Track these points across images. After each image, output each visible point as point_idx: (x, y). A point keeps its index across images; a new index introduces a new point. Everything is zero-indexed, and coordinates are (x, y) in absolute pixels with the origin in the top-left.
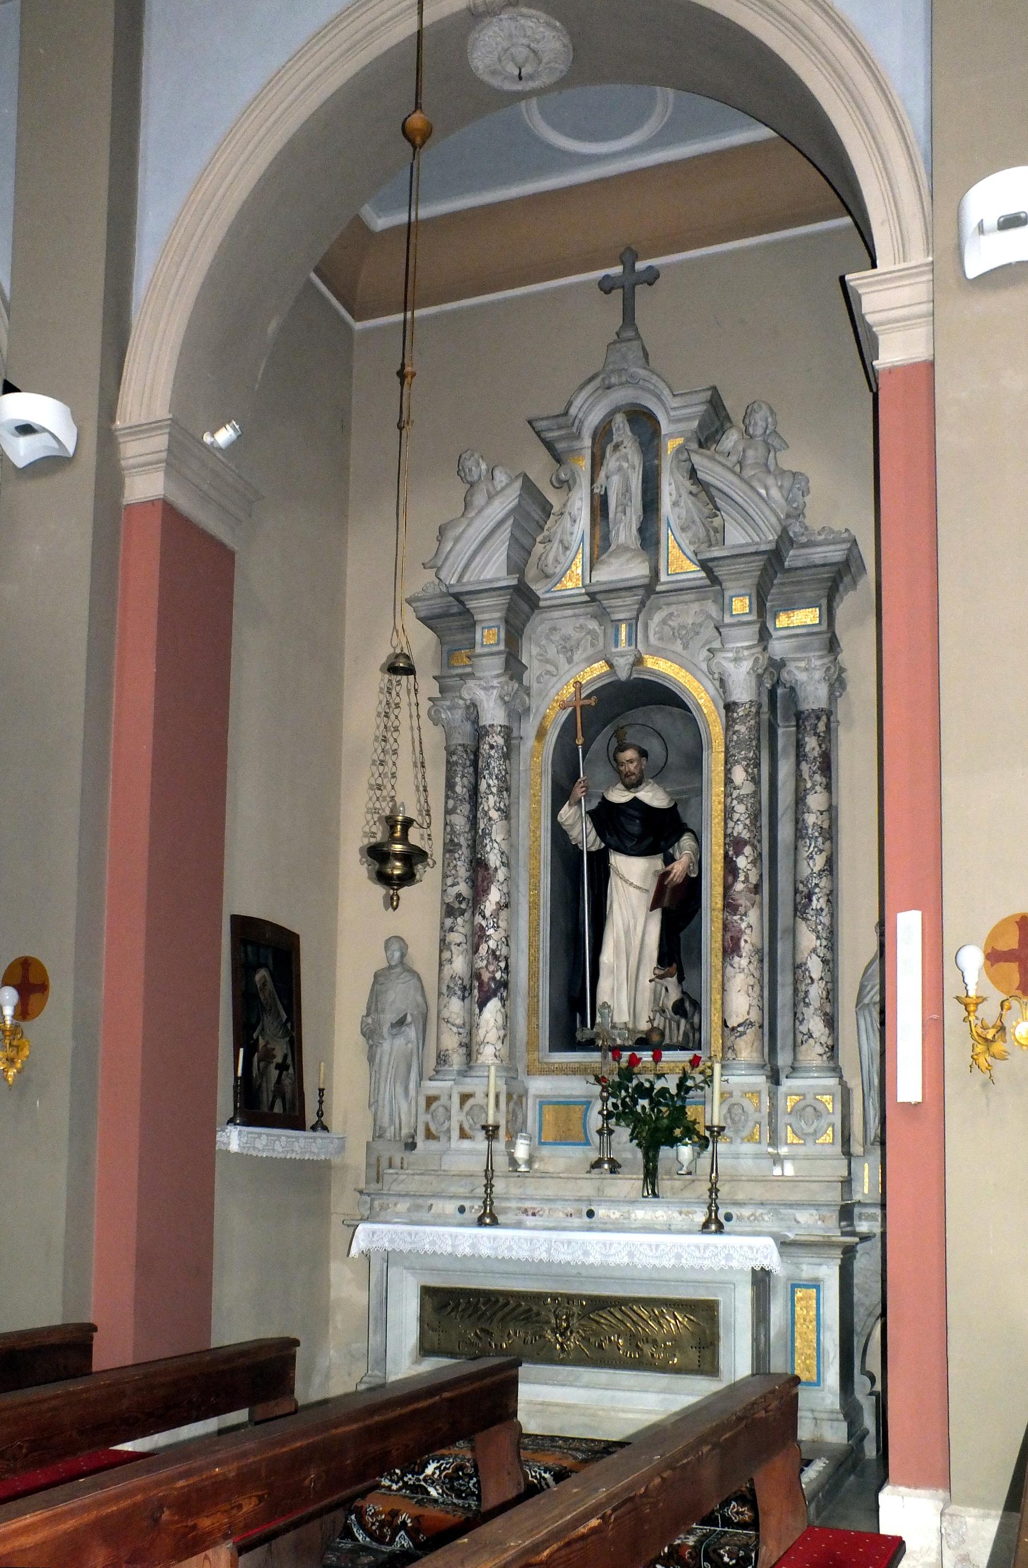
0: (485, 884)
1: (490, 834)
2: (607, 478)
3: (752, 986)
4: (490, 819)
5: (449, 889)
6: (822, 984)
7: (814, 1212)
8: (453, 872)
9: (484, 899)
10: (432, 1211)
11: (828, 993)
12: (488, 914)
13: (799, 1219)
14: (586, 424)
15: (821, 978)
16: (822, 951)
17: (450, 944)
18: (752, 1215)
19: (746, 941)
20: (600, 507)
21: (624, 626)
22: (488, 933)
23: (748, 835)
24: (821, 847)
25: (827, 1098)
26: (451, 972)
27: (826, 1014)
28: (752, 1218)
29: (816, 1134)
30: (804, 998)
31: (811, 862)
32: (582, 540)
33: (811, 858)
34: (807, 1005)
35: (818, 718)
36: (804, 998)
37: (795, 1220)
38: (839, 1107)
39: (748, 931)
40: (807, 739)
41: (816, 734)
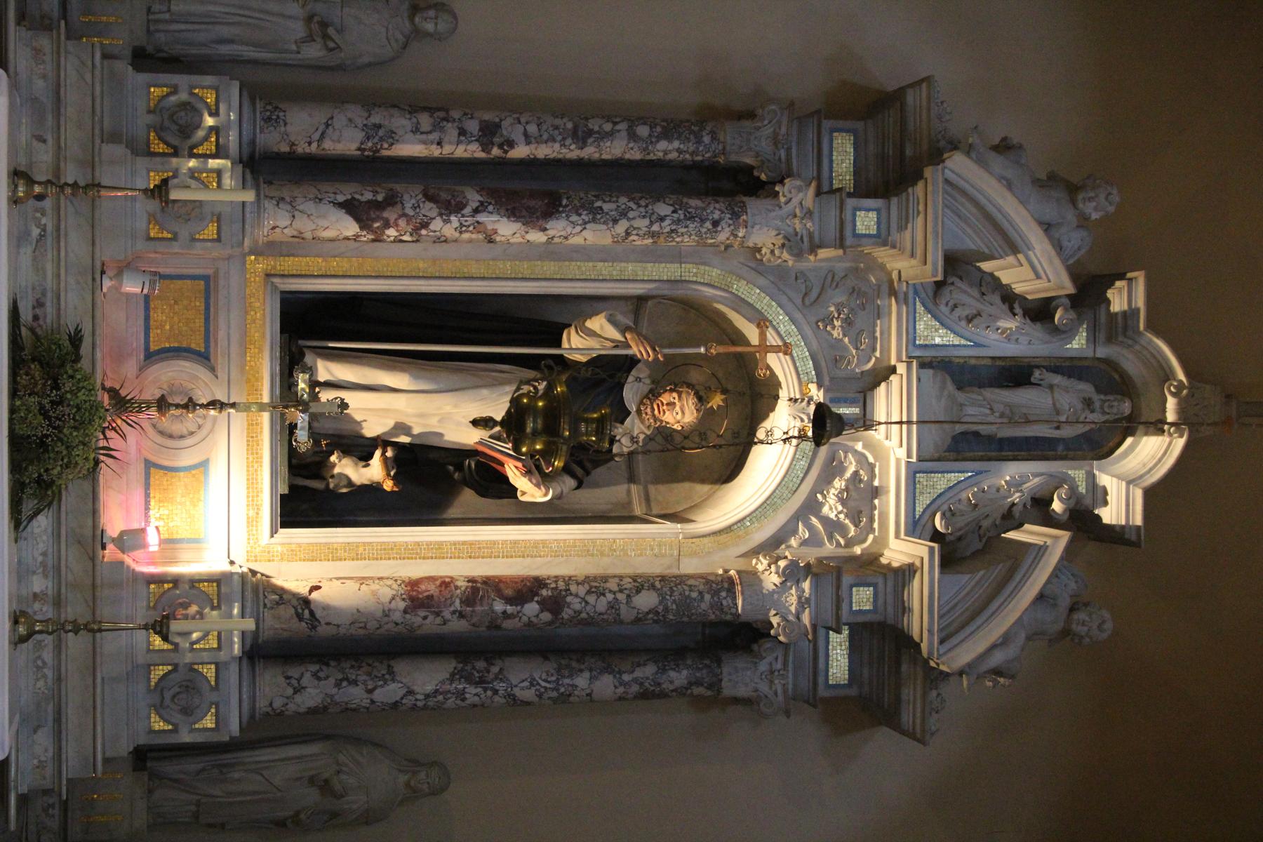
0: (524, 213)
1: (594, 220)
2: (1051, 387)
3: (365, 628)
4: (615, 221)
5: (520, 128)
6: (366, 703)
7: (50, 754)
8: (545, 136)
9: (503, 211)
10: (35, 143)
11: (354, 710)
12: (482, 218)
13: (40, 733)
14: (1125, 352)
15: (373, 702)
16: (408, 701)
17: (442, 129)
18: (44, 663)
19: (425, 618)
20: (1015, 374)
21: (857, 410)
22: (453, 218)
23: (566, 617)
24: (546, 696)
25: (209, 722)
26: (400, 132)
27: (325, 708)
28: (39, 663)
29: (160, 708)
30: (347, 679)
31: (526, 684)
32: (977, 345)
33: (532, 685)
34: (338, 685)
35: (710, 687)
36: (347, 679)
37: (39, 727)
38: (199, 738)
39: (438, 620)
40: (685, 672)
41: (690, 684)
